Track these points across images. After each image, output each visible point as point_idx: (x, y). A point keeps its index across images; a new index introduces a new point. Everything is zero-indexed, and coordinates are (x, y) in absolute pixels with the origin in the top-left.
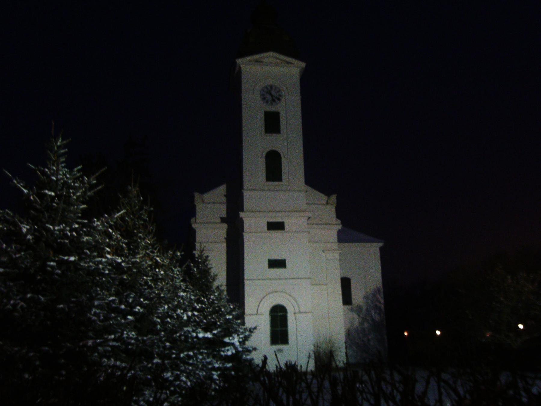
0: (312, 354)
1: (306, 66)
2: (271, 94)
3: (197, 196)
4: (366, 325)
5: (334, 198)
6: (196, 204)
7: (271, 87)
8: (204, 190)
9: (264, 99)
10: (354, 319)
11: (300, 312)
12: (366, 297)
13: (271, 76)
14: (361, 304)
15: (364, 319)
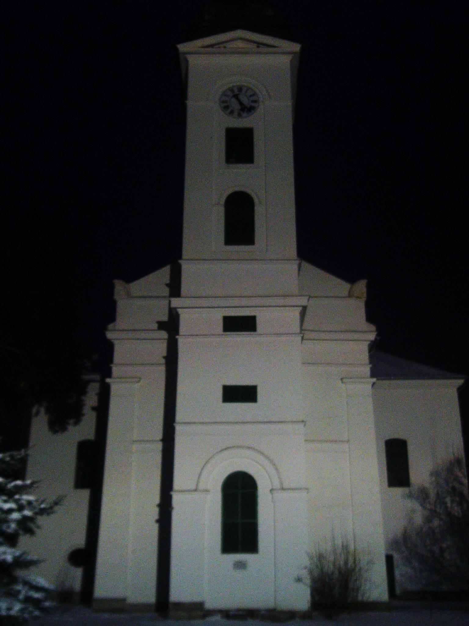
0: (305, 574)
1: (302, 49)
2: (240, 100)
3: (119, 286)
4: (436, 522)
5: (361, 286)
6: (116, 297)
7: (240, 89)
8: (131, 276)
9: (226, 108)
10: (413, 511)
11: (283, 489)
12: (435, 474)
13: (239, 72)
14: (427, 485)
15: (433, 513)
